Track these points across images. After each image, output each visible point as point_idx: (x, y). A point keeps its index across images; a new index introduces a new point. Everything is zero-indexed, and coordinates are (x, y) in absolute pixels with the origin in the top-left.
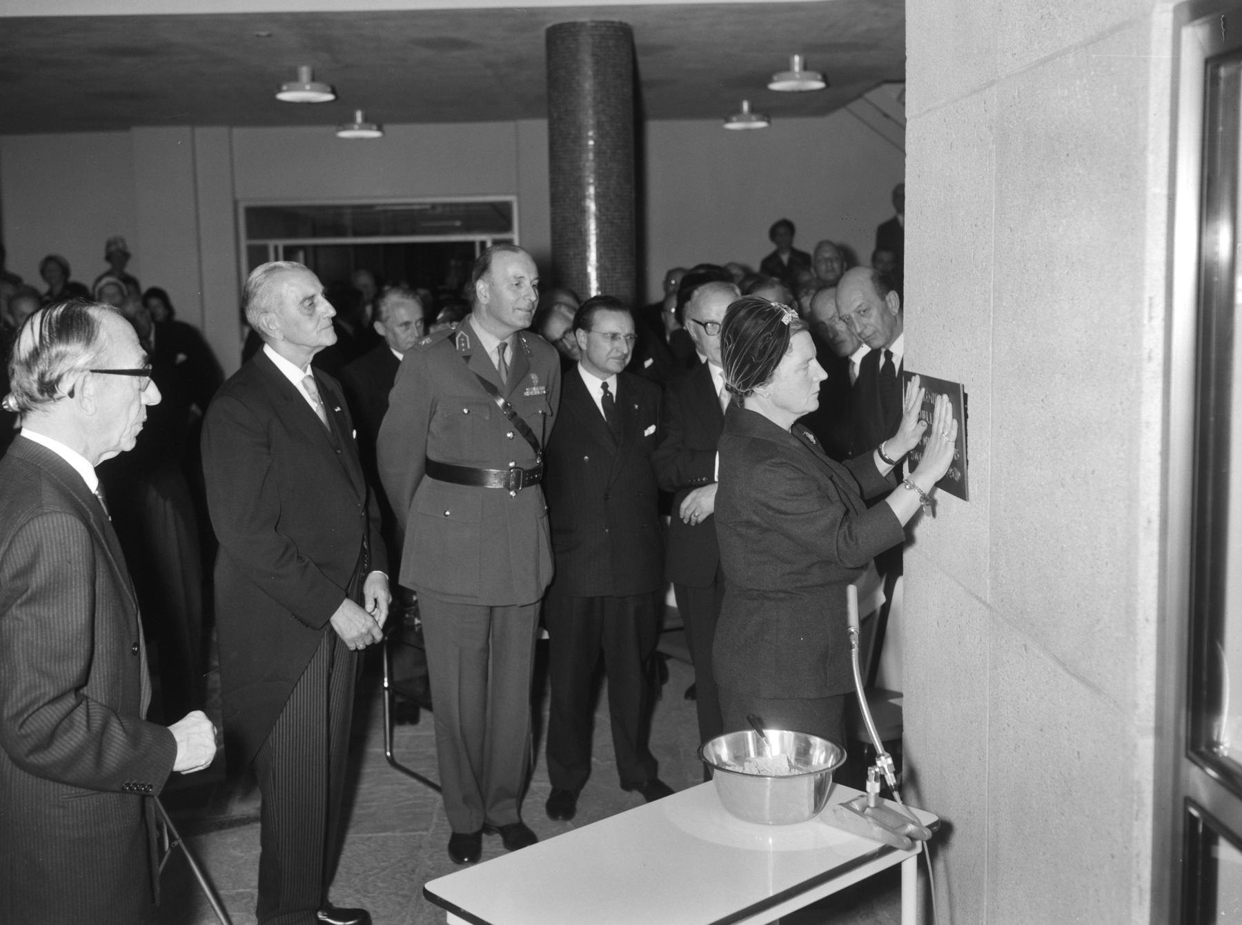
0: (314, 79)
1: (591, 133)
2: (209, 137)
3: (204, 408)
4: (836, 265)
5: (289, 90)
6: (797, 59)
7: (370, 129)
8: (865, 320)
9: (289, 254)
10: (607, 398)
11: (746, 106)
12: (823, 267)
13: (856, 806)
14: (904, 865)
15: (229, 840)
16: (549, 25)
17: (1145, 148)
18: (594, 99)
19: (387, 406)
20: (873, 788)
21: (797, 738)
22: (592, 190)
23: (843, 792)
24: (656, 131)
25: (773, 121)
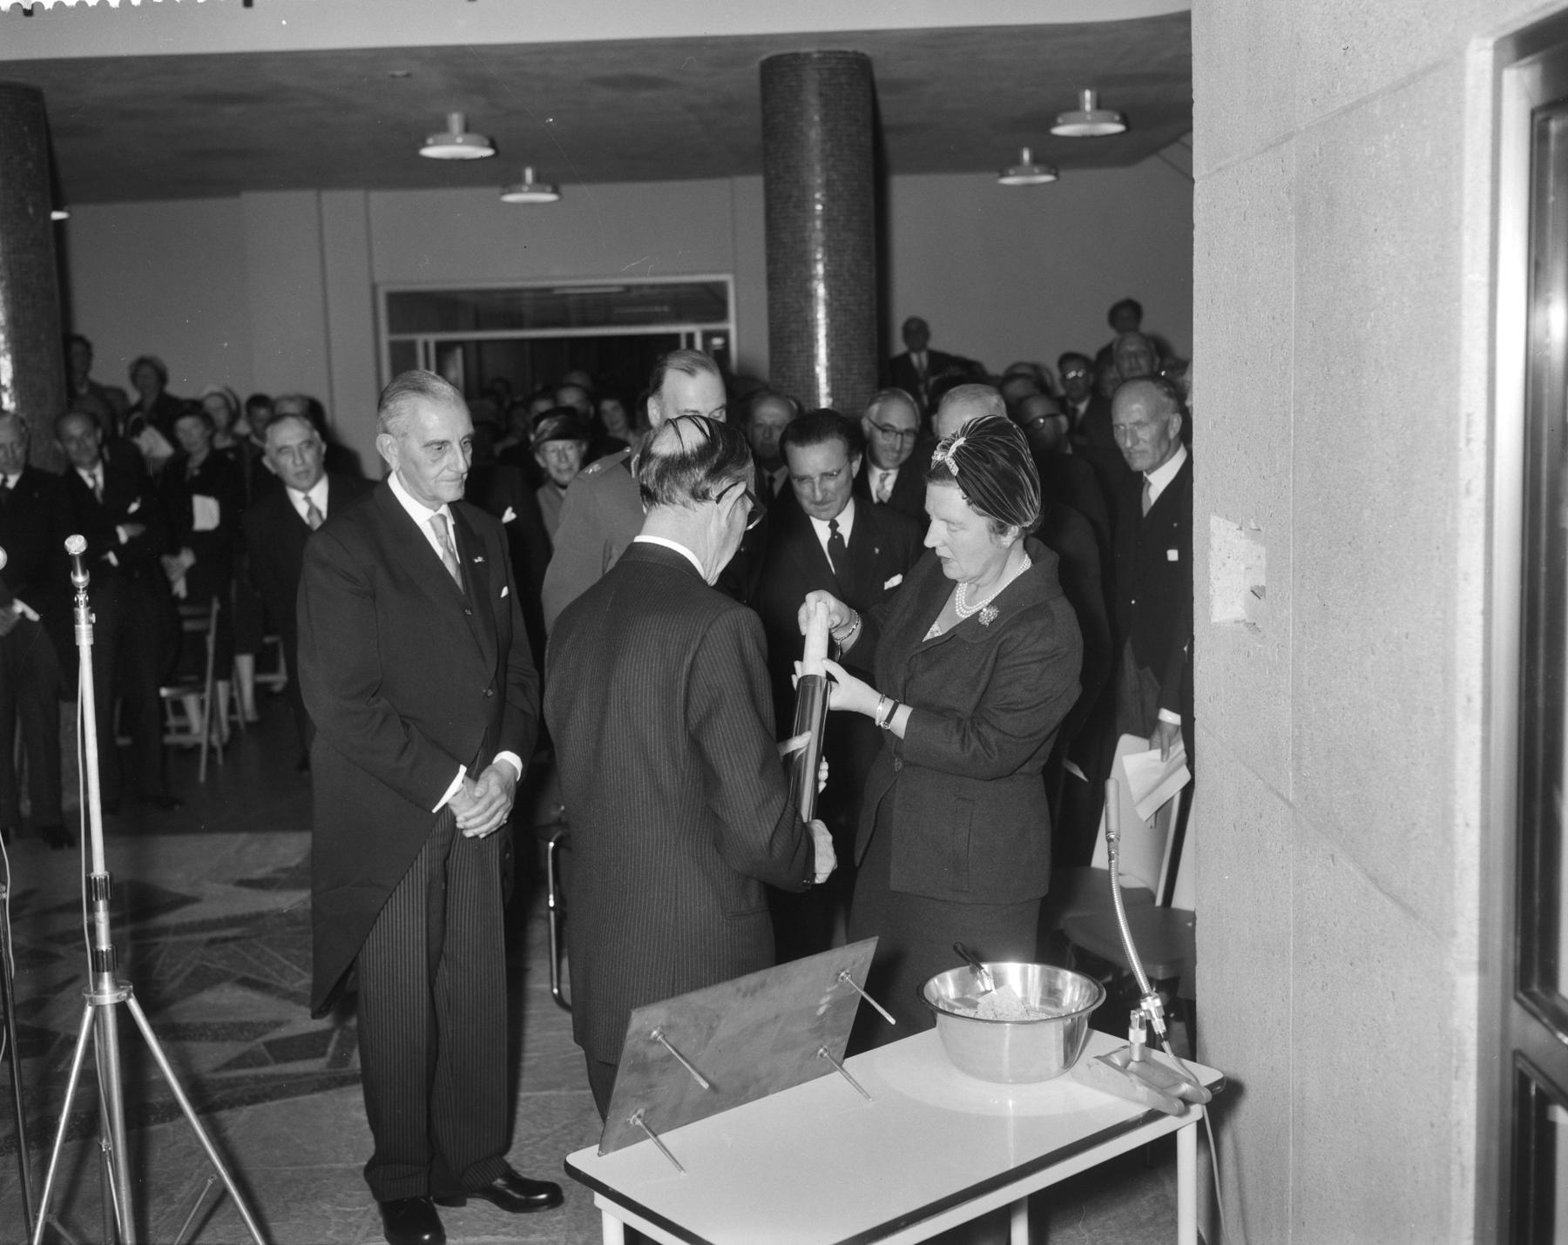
1: (818, 196)
2: (342, 203)
4: (1143, 362)
5: (435, 144)
6: (1088, 94)
7: (543, 191)
10: (836, 538)
12: (1126, 365)
14: (1180, 1135)
16: (764, 57)
18: (823, 151)
22: (820, 269)
23: (1102, 1042)
24: (905, 190)
25: (1062, 174)
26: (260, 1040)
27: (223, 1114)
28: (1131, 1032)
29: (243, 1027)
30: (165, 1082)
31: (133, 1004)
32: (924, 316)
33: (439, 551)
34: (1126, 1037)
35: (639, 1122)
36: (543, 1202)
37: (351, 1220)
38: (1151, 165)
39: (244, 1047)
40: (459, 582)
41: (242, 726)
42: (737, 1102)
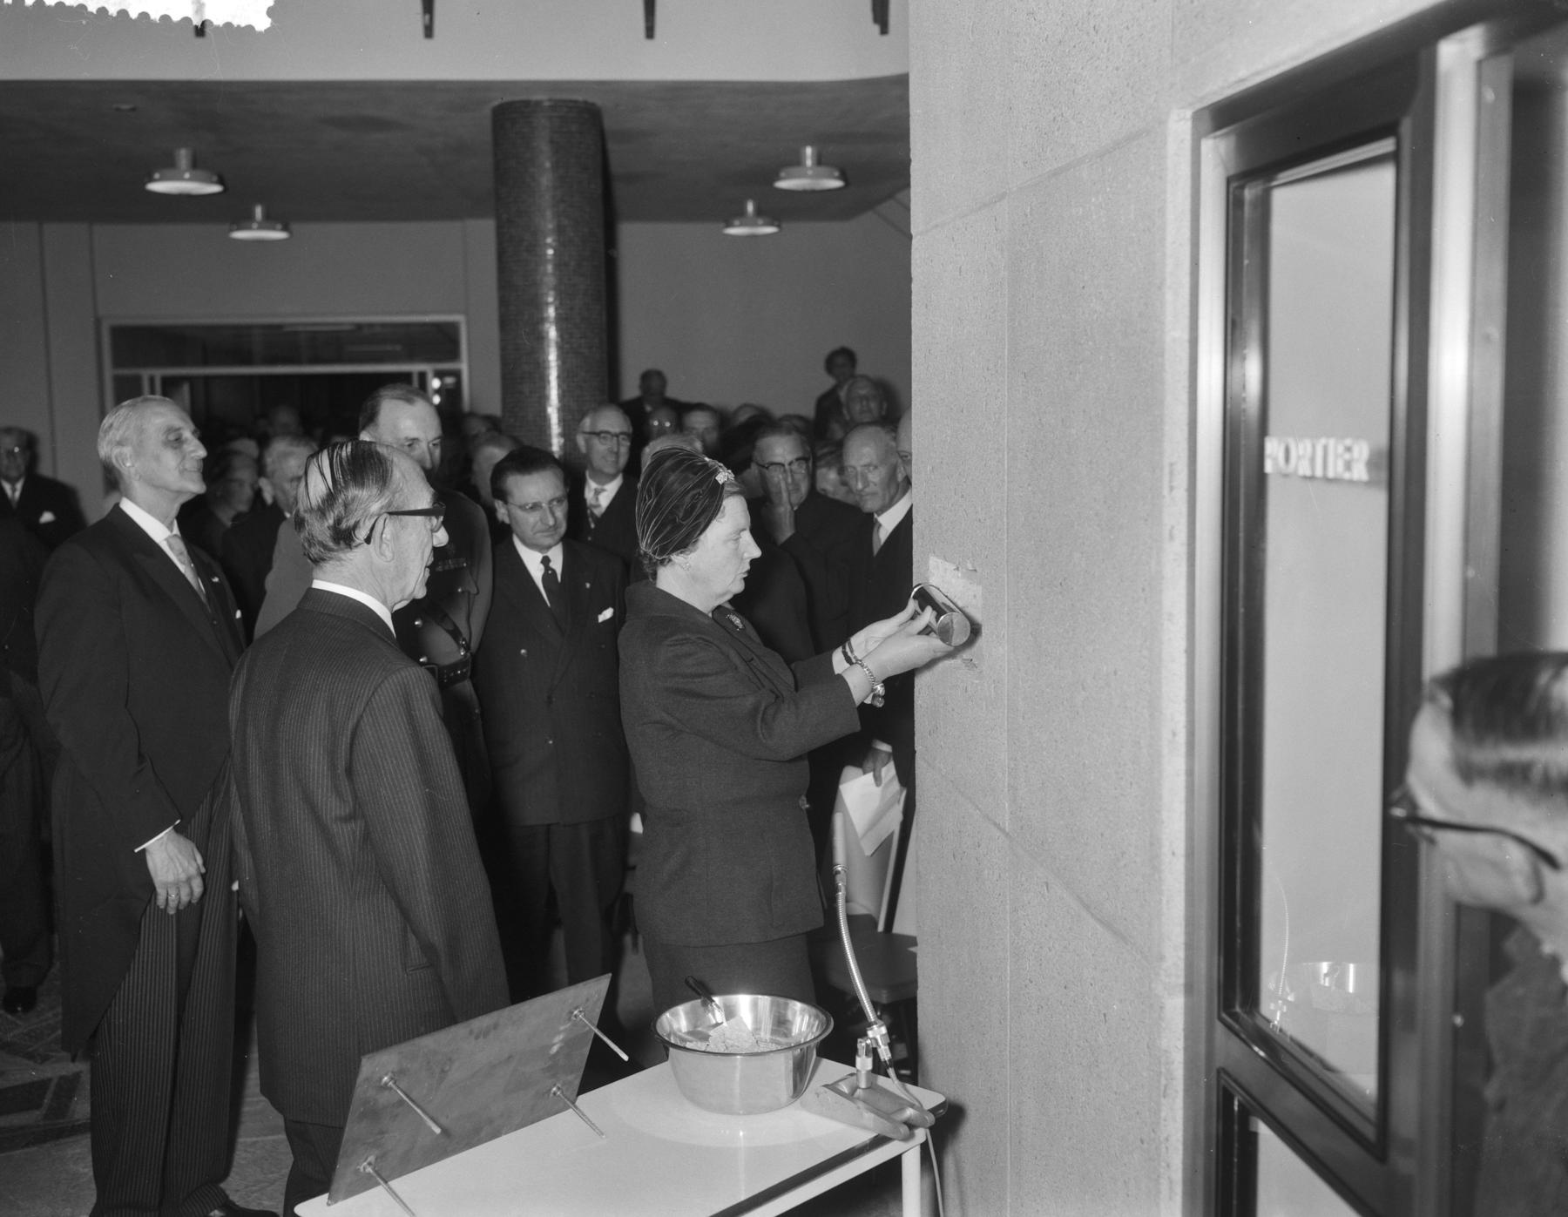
1: (549, 240)
3: (846, 433)
5: (161, 179)
6: (809, 151)
7: (274, 229)
9: (169, 388)
10: (549, 575)
11: (750, 207)
12: (857, 407)
16: (496, 103)
19: (264, 593)
20: (863, 1065)
21: (772, 1004)
22: (551, 312)
23: (831, 1070)
24: (634, 238)
28: (858, 1060)
34: (853, 1064)
35: (369, 1170)
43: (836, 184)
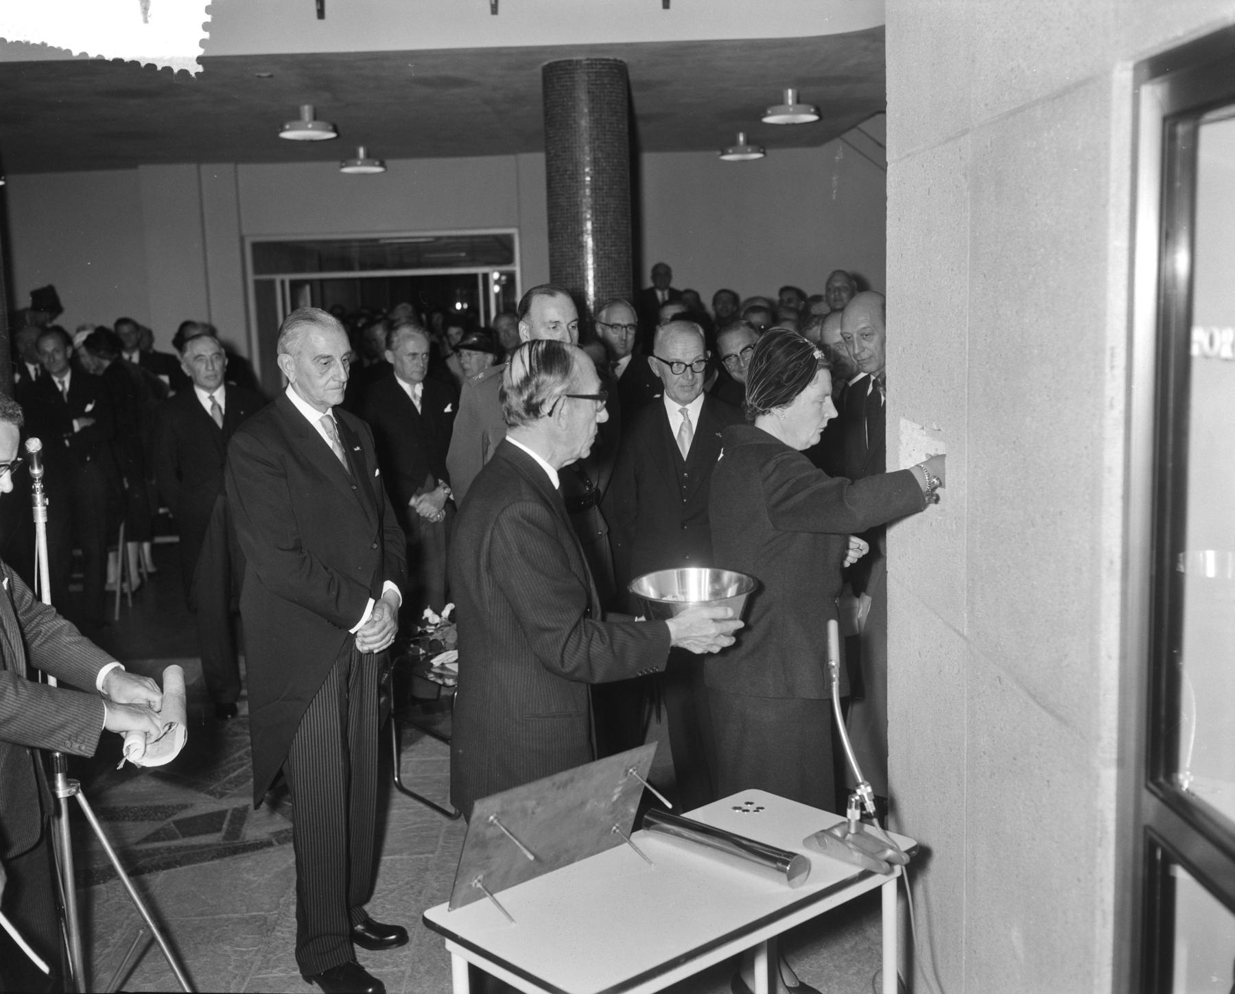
0: (316, 117)
1: (587, 170)
2: (215, 174)
6: (790, 92)
7: (374, 165)
8: (865, 344)
10: (215, 404)
13: (838, 833)
15: (243, 865)
17: (1107, 201)
20: (853, 815)
22: (589, 225)
24: (651, 163)
26: (170, 820)
27: (147, 877)
28: (849, 811)
29: (157, 809)
30: (104, 852)
31: (81, 798)
32: (667, 262)
33: (330, 443)
34: (845, 815)
35: (479, 885)
36: (392, 943)
37: (246, 957)
38: (837, 151)
39: (158, 825)
40: (346, 466)
41: (145, 576)
42: (552, 869)
43: (814, 118)
